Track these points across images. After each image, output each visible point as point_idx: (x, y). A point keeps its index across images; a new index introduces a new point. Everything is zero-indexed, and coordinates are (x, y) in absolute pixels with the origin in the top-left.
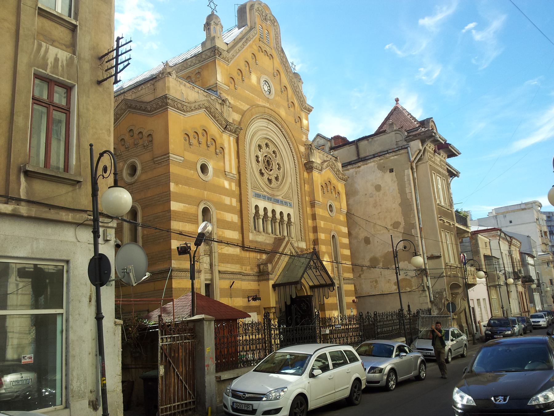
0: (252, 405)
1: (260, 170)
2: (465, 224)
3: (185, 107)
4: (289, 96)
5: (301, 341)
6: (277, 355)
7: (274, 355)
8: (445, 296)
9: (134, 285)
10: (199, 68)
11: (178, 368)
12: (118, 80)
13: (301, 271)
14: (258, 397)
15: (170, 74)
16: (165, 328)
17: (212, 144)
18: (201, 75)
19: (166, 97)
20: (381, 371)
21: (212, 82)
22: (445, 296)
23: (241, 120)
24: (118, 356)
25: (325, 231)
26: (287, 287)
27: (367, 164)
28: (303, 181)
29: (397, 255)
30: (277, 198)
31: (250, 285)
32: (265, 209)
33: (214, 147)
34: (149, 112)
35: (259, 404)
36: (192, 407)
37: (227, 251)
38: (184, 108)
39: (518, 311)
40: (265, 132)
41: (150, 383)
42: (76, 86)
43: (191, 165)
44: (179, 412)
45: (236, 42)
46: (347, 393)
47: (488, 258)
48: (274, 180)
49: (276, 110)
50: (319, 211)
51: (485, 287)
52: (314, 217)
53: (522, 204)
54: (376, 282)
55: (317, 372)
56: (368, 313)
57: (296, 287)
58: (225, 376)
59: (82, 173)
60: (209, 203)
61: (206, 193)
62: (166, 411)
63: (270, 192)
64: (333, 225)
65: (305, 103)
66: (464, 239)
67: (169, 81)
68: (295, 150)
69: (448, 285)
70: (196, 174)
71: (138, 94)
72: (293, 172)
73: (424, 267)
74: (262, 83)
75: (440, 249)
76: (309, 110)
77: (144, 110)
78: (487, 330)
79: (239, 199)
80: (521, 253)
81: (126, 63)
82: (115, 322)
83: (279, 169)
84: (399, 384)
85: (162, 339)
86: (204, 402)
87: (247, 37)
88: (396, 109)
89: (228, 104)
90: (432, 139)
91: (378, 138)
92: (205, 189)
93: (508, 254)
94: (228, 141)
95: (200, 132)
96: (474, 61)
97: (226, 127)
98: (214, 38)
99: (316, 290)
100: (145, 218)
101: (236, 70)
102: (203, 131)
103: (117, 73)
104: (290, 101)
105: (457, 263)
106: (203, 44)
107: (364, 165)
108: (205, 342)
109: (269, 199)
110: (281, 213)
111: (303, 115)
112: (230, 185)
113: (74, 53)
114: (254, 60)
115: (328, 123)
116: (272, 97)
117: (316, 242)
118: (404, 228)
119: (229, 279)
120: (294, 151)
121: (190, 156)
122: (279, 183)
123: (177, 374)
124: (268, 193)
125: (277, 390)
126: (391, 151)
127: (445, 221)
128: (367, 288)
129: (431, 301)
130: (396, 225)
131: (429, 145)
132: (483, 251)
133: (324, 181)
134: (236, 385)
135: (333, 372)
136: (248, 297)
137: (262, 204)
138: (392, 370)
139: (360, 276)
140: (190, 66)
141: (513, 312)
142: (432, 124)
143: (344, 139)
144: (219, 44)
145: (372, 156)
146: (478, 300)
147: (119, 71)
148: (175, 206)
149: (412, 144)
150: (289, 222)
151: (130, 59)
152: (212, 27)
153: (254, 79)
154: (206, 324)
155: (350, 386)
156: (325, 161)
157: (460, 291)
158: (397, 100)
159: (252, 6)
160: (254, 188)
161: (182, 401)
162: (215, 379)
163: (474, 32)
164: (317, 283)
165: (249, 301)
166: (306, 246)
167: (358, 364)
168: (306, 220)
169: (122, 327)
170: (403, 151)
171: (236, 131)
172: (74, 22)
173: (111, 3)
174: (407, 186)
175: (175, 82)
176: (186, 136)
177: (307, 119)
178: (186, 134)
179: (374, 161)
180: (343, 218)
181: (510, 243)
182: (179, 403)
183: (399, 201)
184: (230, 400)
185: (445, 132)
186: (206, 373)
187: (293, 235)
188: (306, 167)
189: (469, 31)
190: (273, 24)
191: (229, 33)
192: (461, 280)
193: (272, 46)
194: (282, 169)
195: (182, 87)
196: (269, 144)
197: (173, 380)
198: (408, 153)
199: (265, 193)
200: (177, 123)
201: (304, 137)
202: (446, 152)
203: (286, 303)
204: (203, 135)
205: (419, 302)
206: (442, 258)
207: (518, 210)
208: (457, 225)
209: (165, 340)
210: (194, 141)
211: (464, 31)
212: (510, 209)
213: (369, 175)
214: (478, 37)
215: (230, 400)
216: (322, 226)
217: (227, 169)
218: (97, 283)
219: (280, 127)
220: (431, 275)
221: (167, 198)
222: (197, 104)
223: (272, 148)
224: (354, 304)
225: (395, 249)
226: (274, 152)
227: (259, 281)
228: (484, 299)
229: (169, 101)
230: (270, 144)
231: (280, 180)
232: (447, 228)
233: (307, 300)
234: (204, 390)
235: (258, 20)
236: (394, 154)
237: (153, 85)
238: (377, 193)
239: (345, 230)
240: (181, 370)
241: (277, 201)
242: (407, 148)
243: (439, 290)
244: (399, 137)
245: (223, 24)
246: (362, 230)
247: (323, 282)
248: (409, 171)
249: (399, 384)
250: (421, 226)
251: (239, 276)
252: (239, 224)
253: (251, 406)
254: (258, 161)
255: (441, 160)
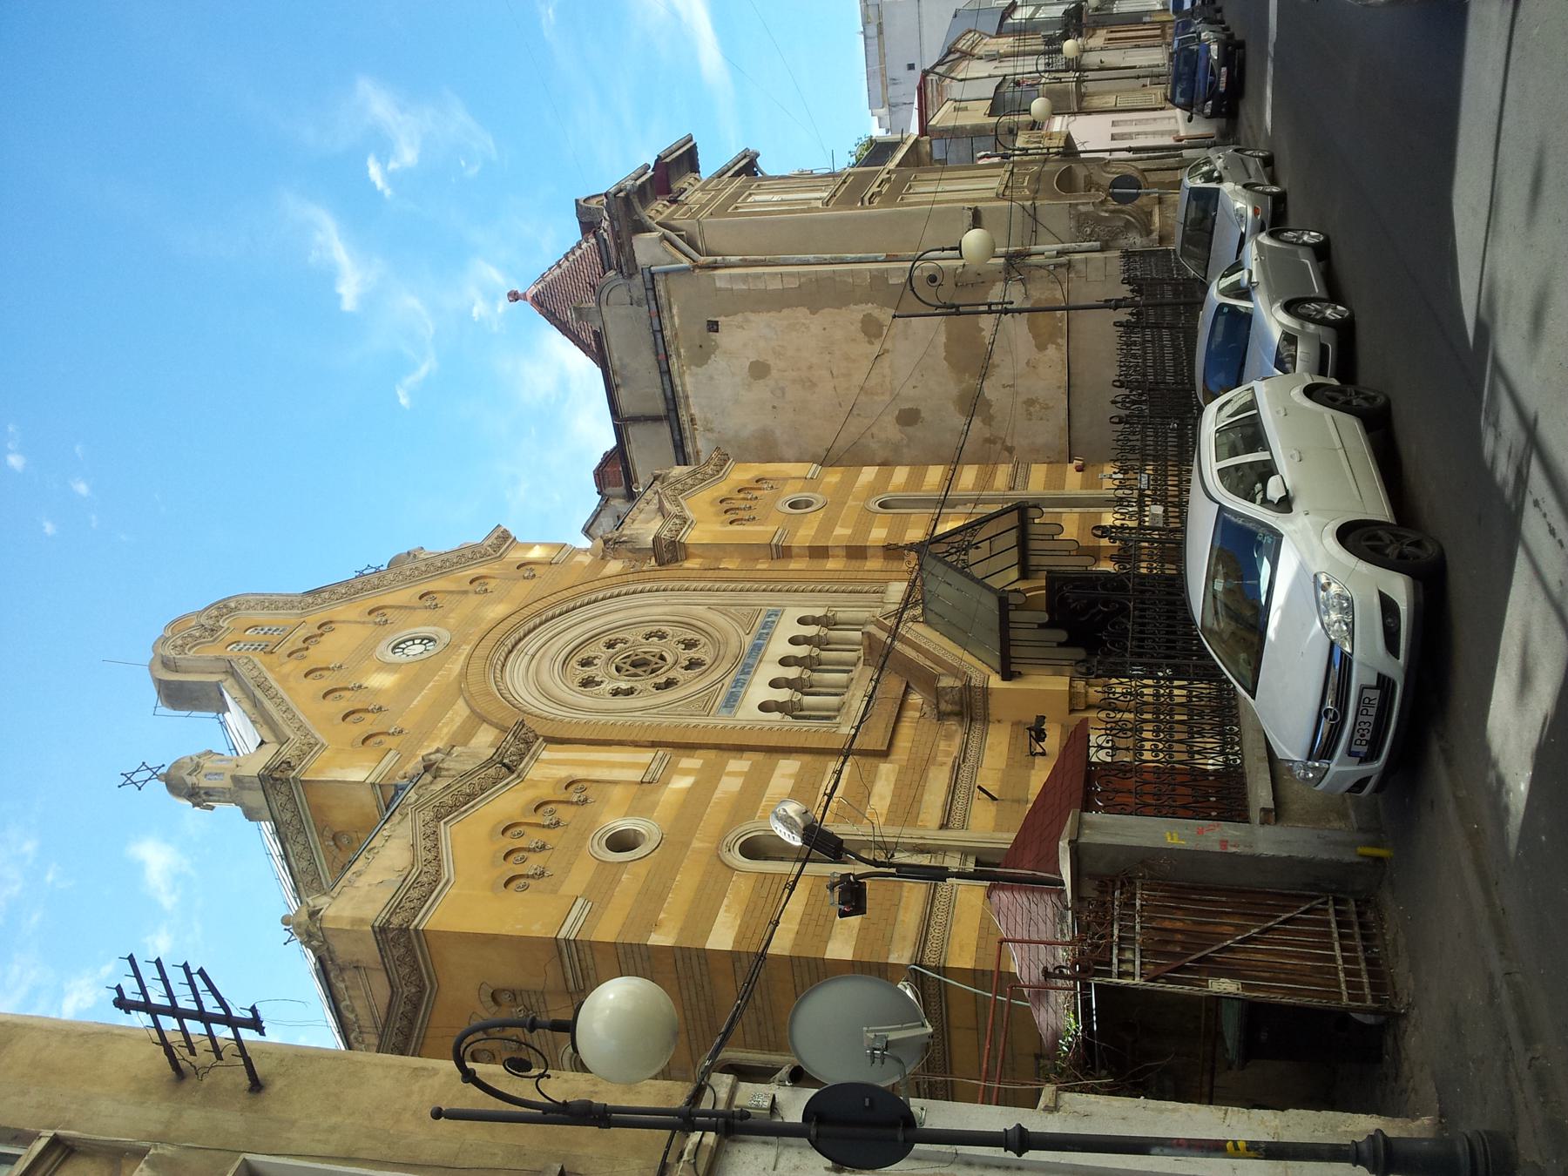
0: (1363, 689)
1: (658, 687)
2: (891, 147)
3: (424, 879)
4: (453, 587)
5: (1180, 615)
6: (1210, 622)
7: (1211, 631)
8: (1091, 208)
9: (930, 1030)
10: (321, 835)
11: (1224, 936)
12: (250, 1015)
13: (974, 590)
14: (1339, 667)
15: (313, 914)
16: (1090, 963)
17: (552, 812)
18: (343, 833)
19: (381, 931)
20: (1289, 338)
21: (368, 799)
22: (1091, 208)
23: (496, 726)
24: (1161, 1111)
25: (865, 520)
26: (1012, 634)
27: (687, 397)
28: (710, 574)
29: (953, 306)
30: (747, 648)
31: (996, 749)
32: (775, 684)
33: (561, 806)
34: (421, 990)
35: (1361, 664)
36: (1352, 906)
37: (882, 798)
38: (425, 882)
39: (1158, 50)
40: (546, 664)
41: (1264, 1036)
42: (248, 1157)
43: (606, 879)
44: (1366, 949)
45: (260, 717)
46: (1351, 424)
47: (997, 106)
48: (693, 654)
49: (485, 627)
50: (805, 533)
51: (1082, 119)
52: (819, 552)
53: (864, 33)
54: (1030, 402)
55: (1274, 490)
56: (1114, 402)
57: (1018, 608)
58: (1261, 794)
59: (537, 1166)
60: (729, 839)
61: (696, 844)
62: (1360, 986)
63: (725, 666)
64: (851, 502)
65: (480, 545)
66: (937, 156)
67: (335, 919)
68: (617, 585)
69: (1059, 197)
70: (633, 869)
71: (366, 1021)
72: (673, 597)
73: (1002, 260)
74: (398, 657)
75: (955, 209)
76: (503, 538)
77: (416, 1007)
78: (1202, 111)
79: (733, 754)
80: (999, 34)
81: (200, 985)
82: (1047, 1109)
83: (662, 636)
84: (1334, 294)
85: (1121, 975)
86: (1338, 865)
87: (251, 684)
88: (539, 302)
89: (439, 756)
90: (636, 201)
91: (615, 356)
92: (687, 845)
93: (996, 63)
94: (550, 768)
95: (509, 843)
96: (473, 172)
97: (509, 768)
98: (236, 780)
99: (1034, 560)
100: (748, 1038)
101: (343, 724)
102: (509, 833)
103: (228, 1020)
104: (466, 586)
105: (1002, 171)
106: (250, 815)
107: (688, 406)
108: (1149, 844)
109: (747, 670)
110: (794, 641)
111: (515, 556)
112: (686, 772)
113: (140, 1154)
114: (325, 673)
115: (553, 502)
116: (444, 635)
117: (892, 551)
118: (883, 305)
119: (969, 801)
120: (616, 591)
121: (578, 879)
122: (703, 640)
123: (1240, 942)
124: (728, 672)
125: (1322, 608)
126: (656, 321)
127: (875, 189)
128: (1049, 430)
129: (1102, 250)
130: (871, 329)
131: (653, 213)
132: (978, 115)
133: (717, 514)
134: (1292, 743)
135: (1279, 449)
136: (1033, 754)
137: (759, 690)
138: (1289, 307)
139: (1010, 450)
140: (312, 861)
141: (1160, 62)
142: (594, 201)
143: (608, 458)
144: (253, 768)
145: (666, 378)
146: (1113, 138)
147: (221, 1012)
148: (722, 937)
149: (642, 258)
150: (827, 622)
151: (186, 967)
152: (204, 783)
153: (381, 681)
154: (1088, 837)
155: (1328, 413)
156: (661, 509)
157: (1080, 172)
158: (514, 296)
159: (167, 664)
160: (706, 708)
161: (1329, 935)
162: (1267, 828)
163: (392, 165)
164: (1013, 556)
165: (1043, 754)
166: (900, 580)
167: (1262, 390)
168: (825, 575)
169: (1071, 1090)
170: (660, 287)
171: (523, 740)
172: (39, 1146)
173: (16, 1026)
174: (761, 286)
175: (340, 899)
176: (513, 885)
177: (530, 546)
178: (506, 885)
179: (681, 376)
180: (833, 477)
181: (967, 55)
182: (1337, 945)
183: (802, 313)
184: (1340, 767)
185: (621, 160)
186: (1248, 851)
187: (863, 615)
188: (669, 562)
189: (391, 178)
190: (232, 610)
191: (236, 737)
192: (1048, 167)
193: (294, 621)
194: (664, 628)
195: (362, 882)
196: (585, 656)
197: (1259, 957)
198: (666, 273)
199: (727, 681)
200: (469, 906)
201: (579, 558)
202: (681, 175)
203: (1060, 645)
204: (521, 835)
205: (1102, 275)
206: (979, 205)
207: (881, 45)
208: (891, 165)
209: (1124, 967)
210: (534, 863)
211: (388, 192)
212: (877, 67)
213: (717, 392)
214: (408, 156)
215: (1340, 767)
216: (848, 532)
217: (636, 775)
218: (900, 1137)
219: (537, 620)
220: (1026, 241)
221: (694, 959)
222: (421, 843)
223: (597, 650)
224: (1089, 470)
225: (932, 311)
226: (610, 645)
227: (986, 720)
228: (1114, 124)
229: (396, 921)
230: (584, 654)
231: (697, 637)
232: (897, 189)
233: (1057, 582)
234: (1302, 861)
235: (211, 651)
236: (665, 314)
237: (342, 970)
238: (774, 372)
239: (868, 474)
240: (1231, 930)
241: (757, 649)
242: (652, 275)
243: (1073, 223)
244: (620, 294)
245: (202, 750)
246: (874, 430)
247: (1011, 538)
248: (720, 277)
249: (1334, 294)
250: (882, 256)
251: (965, 772)
252: (807, 758)
253: (1367, 693)
254: (630, 692)
255: (702, 189)
